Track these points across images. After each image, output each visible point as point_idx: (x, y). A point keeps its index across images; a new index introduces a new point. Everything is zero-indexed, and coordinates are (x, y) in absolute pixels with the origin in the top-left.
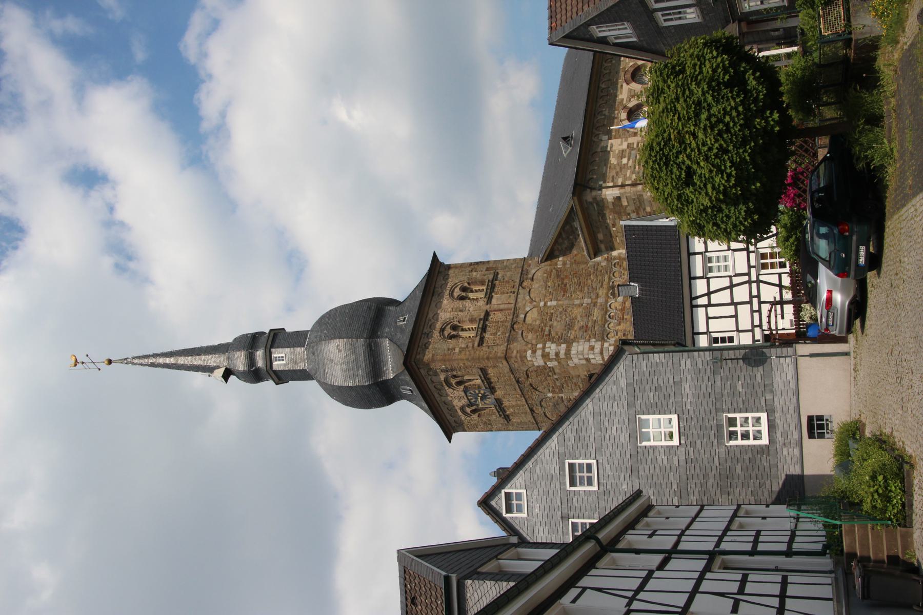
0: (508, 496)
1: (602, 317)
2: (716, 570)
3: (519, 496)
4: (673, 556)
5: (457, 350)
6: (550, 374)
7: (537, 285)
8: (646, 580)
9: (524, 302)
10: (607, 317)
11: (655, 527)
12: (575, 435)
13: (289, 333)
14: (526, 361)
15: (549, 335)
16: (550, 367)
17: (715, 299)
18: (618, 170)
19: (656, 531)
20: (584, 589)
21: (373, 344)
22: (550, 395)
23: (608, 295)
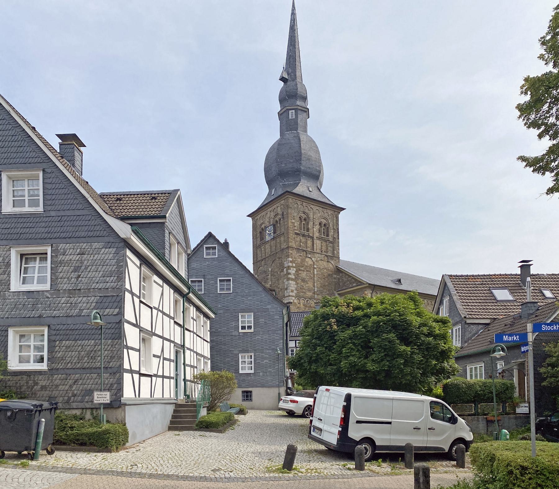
0: (214, 248)
1: (307, 297)
2: (175, 348)
3: (214, 254)
4: (182, 329)
5: (293, 221)
6: (280, 270)
7: (325, 264)
8: (169, 316)
9: (317, 257)
11: (197, 320)
19: (196, 321)
20: (162, 287)
21: (298, 173)
23: (318, 300)
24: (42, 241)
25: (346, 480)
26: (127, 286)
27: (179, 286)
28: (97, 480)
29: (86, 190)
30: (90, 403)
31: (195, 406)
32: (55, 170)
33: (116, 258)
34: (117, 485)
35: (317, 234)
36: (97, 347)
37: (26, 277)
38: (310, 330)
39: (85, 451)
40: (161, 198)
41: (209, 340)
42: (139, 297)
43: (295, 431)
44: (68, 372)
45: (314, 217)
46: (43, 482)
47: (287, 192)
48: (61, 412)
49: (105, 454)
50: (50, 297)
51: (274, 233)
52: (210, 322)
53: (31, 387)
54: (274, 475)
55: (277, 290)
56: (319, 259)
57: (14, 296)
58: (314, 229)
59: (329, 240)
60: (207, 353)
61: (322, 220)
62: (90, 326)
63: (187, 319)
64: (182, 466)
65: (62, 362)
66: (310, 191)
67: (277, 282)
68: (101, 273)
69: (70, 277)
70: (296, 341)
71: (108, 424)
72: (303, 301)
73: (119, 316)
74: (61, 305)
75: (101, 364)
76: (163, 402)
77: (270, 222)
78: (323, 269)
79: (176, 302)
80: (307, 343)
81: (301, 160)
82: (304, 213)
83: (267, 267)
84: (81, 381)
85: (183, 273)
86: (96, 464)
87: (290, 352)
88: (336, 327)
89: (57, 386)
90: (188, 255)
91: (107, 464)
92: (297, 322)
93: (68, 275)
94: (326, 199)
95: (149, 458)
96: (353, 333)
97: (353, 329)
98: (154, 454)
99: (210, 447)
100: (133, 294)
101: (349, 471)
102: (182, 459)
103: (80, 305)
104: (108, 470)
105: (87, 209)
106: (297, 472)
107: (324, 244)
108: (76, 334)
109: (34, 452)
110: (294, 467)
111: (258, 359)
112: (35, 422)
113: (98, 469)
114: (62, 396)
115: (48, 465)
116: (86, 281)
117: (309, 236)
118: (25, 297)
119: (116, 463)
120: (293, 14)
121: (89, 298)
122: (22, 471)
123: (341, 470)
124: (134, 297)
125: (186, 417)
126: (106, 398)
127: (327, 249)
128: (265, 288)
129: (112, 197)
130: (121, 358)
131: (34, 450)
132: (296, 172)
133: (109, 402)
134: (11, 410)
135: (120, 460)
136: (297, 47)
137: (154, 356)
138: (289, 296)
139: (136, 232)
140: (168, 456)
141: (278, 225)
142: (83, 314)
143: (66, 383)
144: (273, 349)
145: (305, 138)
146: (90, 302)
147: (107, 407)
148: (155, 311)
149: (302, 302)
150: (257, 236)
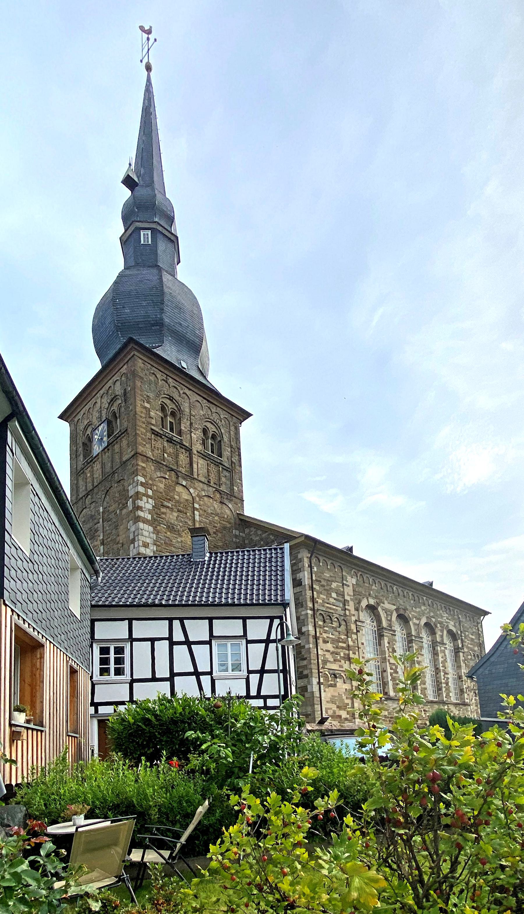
5: (147, 405)
6: (121, 505)
7: (216, 506)
14: (133, 476)
15: (162, 505)
16: (127, 503)
17: (181, 651)
18: (326, 588)
21: (158, 327)
22: (101, 510)
35: (197, 447)
59: (223, 463)
61: (209, 425)
67: (114, 531)
70: (130, 621)
77: (100, 417)
82: (171, 399)
127: (220, 479)
132: (153, 325)
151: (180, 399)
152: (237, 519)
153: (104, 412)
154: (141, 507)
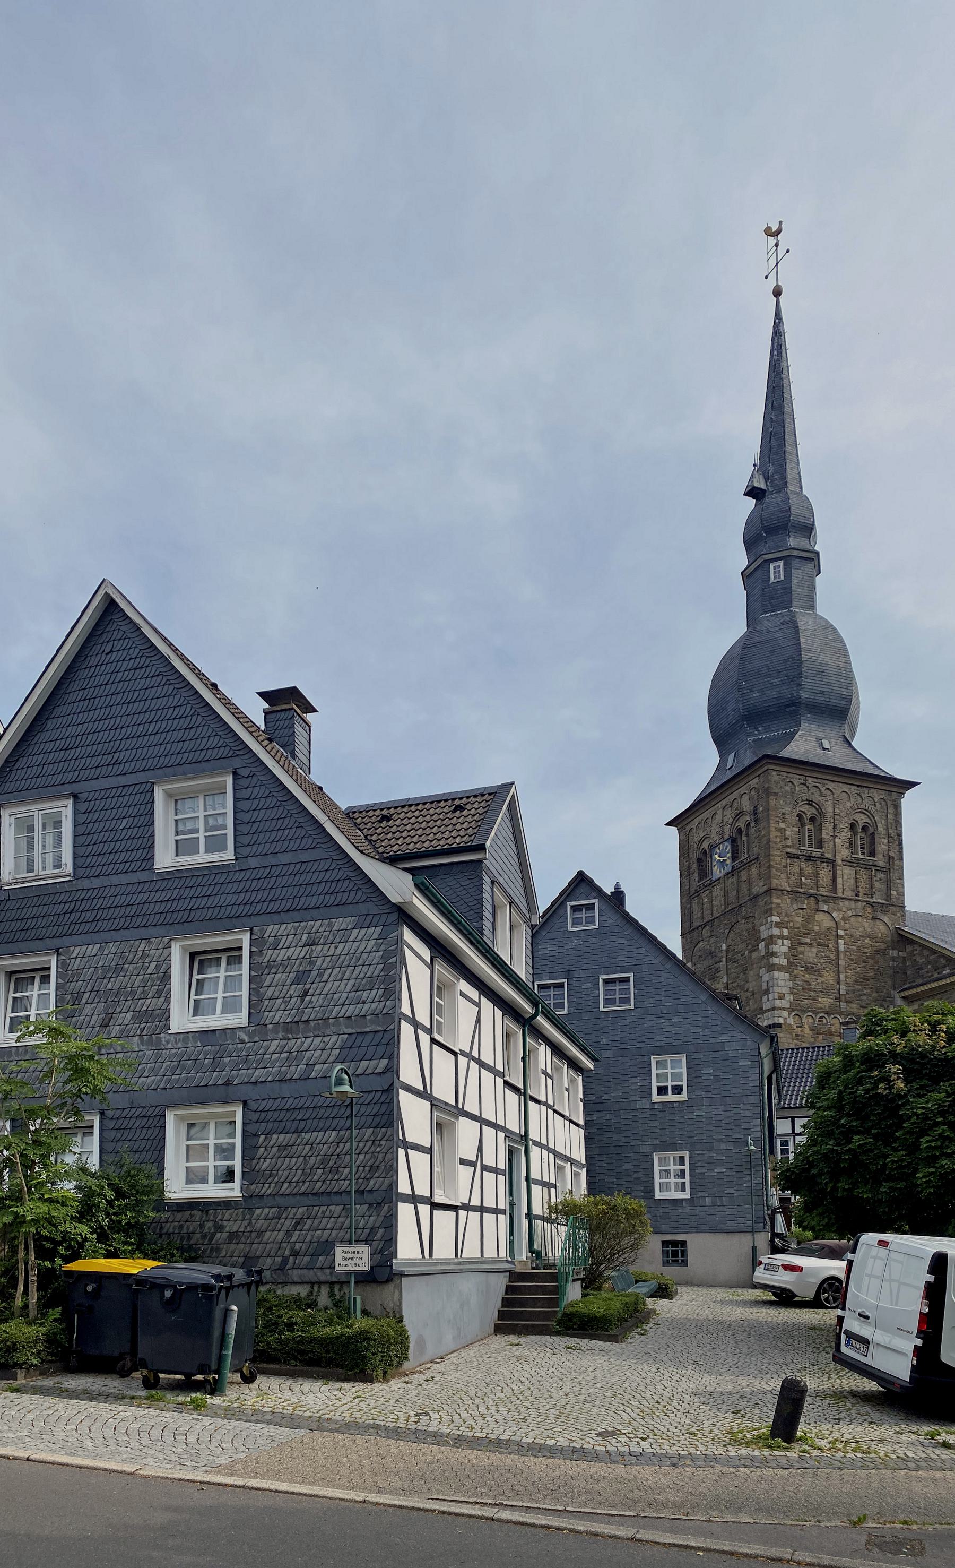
0: (591, 907)
2: (507, 1143)
4: (522, 1097)
5: (782, 825)
6: (750, 947)
7: (866, 925)
8: (492, 1069)
10: (823, 1015)
11: (555, 1077)
12: (663, 984)
13: (813, 581)
15: (799, 943)
16: (758, 945)
19: (551, 1078)
20: (478, 1005)
21: (794, 708)
22: (724, 947)
23: (850, 1014)
24: (231, 922)
25: (938, 1474)
26: (406, 1009)
27: (514, 1001)
28: (344, 1445)
29: (319, 806)
30: (328, 1271)
31: (554, 1277)
32: (259, 769)
33: (383, 948)
34: (389, 1459)
35: (844, 853)
36: (341, 1145)
37: (200, 1000)
38: (833, 1094)
39: (319, 1377)
40: (473, 809)
41: (581, 1122)
42: (429, 1031)
43: (797, 1342)
44: (281, 1201)
45: (837, 811)
46: (235, 1445)
47: (766, 756)
48: (269, 1291)
49: (360, 1386)
50: (247, 1040)
51: (734, 857)
52: (583, 1080)
53: (209, 1235)
54: (751, 1453)
55: (743, 996)
56: (850, 913)
57: (176, 1043)
58: (837, 840)
59: (876, 863)
60: (579, 1154)
61: (858, 817)
62: (328, 1101)
63: (531, 1075)
64: (530, 1420)
65: (270, 1180)
66: (825, 749)
68: (352, 982)
69: (288, 995)
70: (793, 1119)
71: (366, 1318)
72: (811, 1021)
73: (388, 1074)
74: (270, 1056)
75: (350, 1184)
76: (481, 1267)
77: (722, 833)
78: (861, 936)
79: (508, 1037)
80: (828, 1126)
81: (801, 677)
83: (716, 942)
84: (309, 1222)
85: (522, 970)
86: (342, 1409)
87: (779, 1147)
88: (903, 1085)
89: (260, 1233)
90: (533, 927)
91: (365, 1409)
92: (795, 1071)
93: (285, 991)
94: (868, 764)
95: (455, 1398)
96: (950, 1099)
97: (949, 1089)
98: (465, 1390)
99: (592, 1375)
100: (416, 1025)
101: (946, 1452)
102: (529, 1405)
103: (308, 1054)
104: (367, 1422)
105: (323, 846)
106: (807, 1448)
107: (863, 874)
108: (299, 1118)
109: (216, 1376)
110: (799, 1434)
111: (699, 1164)
112: (218, 1313)
113: (347, 1419)
114: (271, 1255)
115: (244, 1407)
116: (320, 1001)
117: (823, 859)
118: (199, 1044)
119: (383, 1407)
120: (778, 333)
121: (326, 1039)
122: (194, 1419)
123: (924, 1446)
124: (419, 1031)
125: (535, 1302)
126: (360, 1259)
128: (713, 995)
129: (371, 814)
130: (392, 1170)
131: (217, 1372)
133: (366, 1268)
134: (173, 1286)
135: (392, 1402)
136: (787, 409)
137: (463, 1162)
138: (774, 1009)
139: (421, 888)
140: (497, 1395)
141: (744, 839)
142: (313, 1075)
143: (279, 1226)
144: (736, 1142)
145: (810, 623)
146: (327, 1047)
147: (364, 1279)
148: (462, 1061)
149: (807, 1021)
150: (692, 870)
151: (821, 799)
152: (896, 936)
153: (727, 829)
154: (776, 953)
